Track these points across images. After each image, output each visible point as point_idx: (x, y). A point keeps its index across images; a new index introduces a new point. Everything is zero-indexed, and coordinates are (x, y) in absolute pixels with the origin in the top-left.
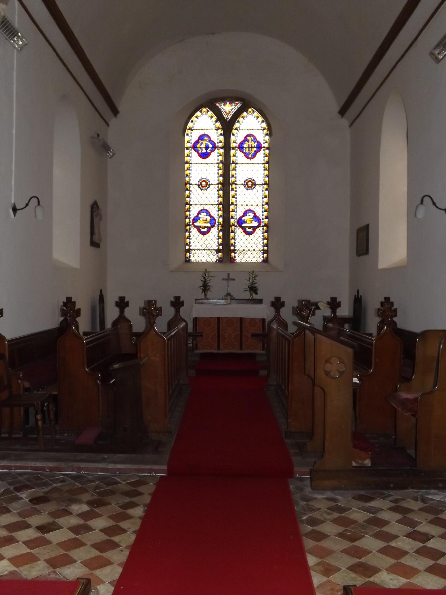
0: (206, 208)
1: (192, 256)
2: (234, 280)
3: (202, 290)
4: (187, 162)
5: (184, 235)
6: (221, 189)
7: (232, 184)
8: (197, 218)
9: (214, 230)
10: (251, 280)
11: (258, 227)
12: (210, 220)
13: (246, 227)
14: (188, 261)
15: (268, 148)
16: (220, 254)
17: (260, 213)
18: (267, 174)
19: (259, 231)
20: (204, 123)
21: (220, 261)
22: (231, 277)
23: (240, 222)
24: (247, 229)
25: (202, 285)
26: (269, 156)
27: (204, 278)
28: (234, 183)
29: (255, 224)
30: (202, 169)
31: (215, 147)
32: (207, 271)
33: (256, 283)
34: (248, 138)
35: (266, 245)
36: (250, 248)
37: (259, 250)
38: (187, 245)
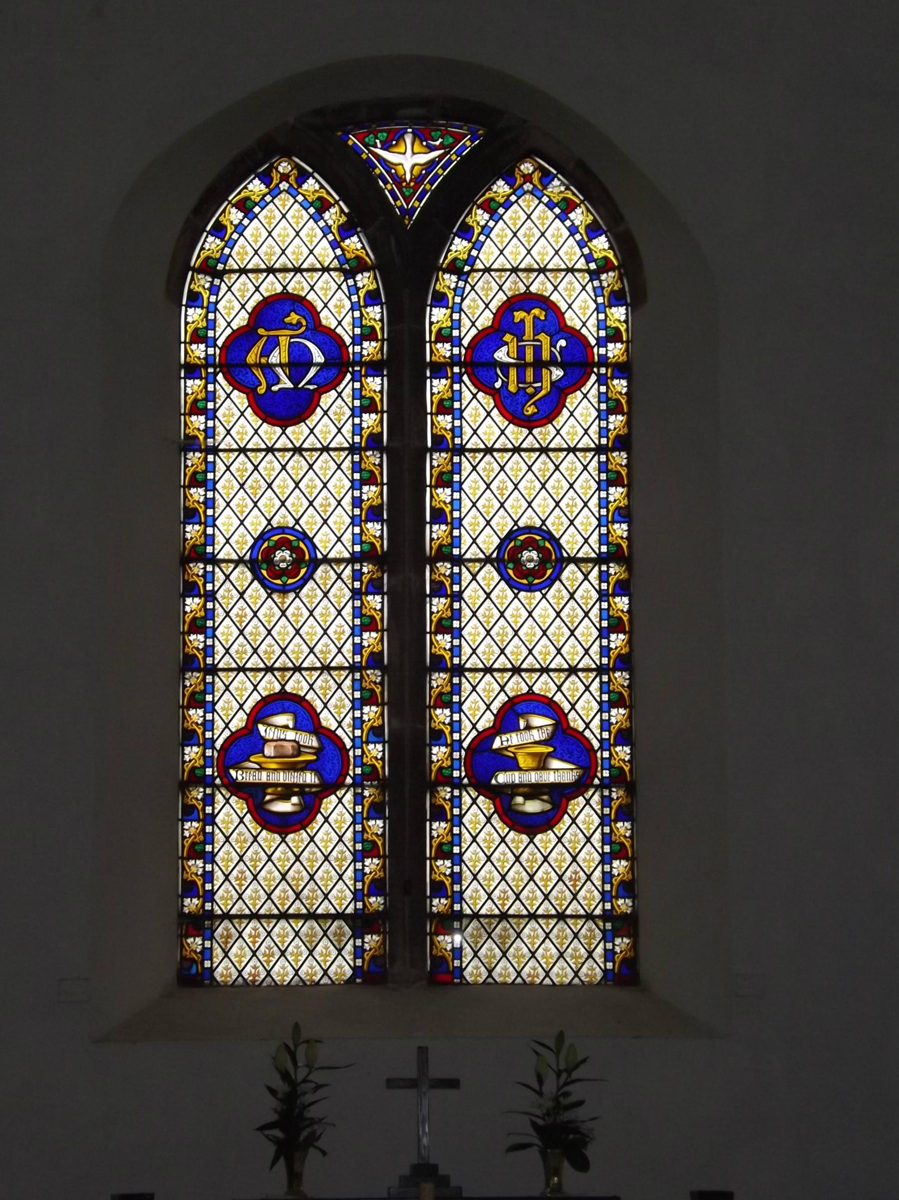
0: (296, 685)
1: (218, 952)
2: (453, 1084)
3: (271, 1149)
4: (191, 444)
5: (173, 833)
6: (375, 587)
7: (433, 561)
8: (246, 742)
9: (338, 809)
10: (550, 1087)
11: (578, 788)
12: (318, 752)
13: (513, 789)
14: (194, 976)
15: (621, 369)
16: (371, 941)
17: (585, 709)
18: (624, 503)
19: (585, 813)
20: (283, 240)
21: (370, 974)
22: (436, 1071)
23: (483, 760)
24: (519, 800)
25: (274, 1117)
26: (630, 406)
27: (285, 1076)
28: (444, 554)
29: (561, 772)
30: (279, 479)
31: (339, 363)
32: (305, 1034)
33: (580, 1103)
34: (519, 315)
35: (627, 888)
36: (533, 895)
37: (589, 917)
38: (190, 889)
